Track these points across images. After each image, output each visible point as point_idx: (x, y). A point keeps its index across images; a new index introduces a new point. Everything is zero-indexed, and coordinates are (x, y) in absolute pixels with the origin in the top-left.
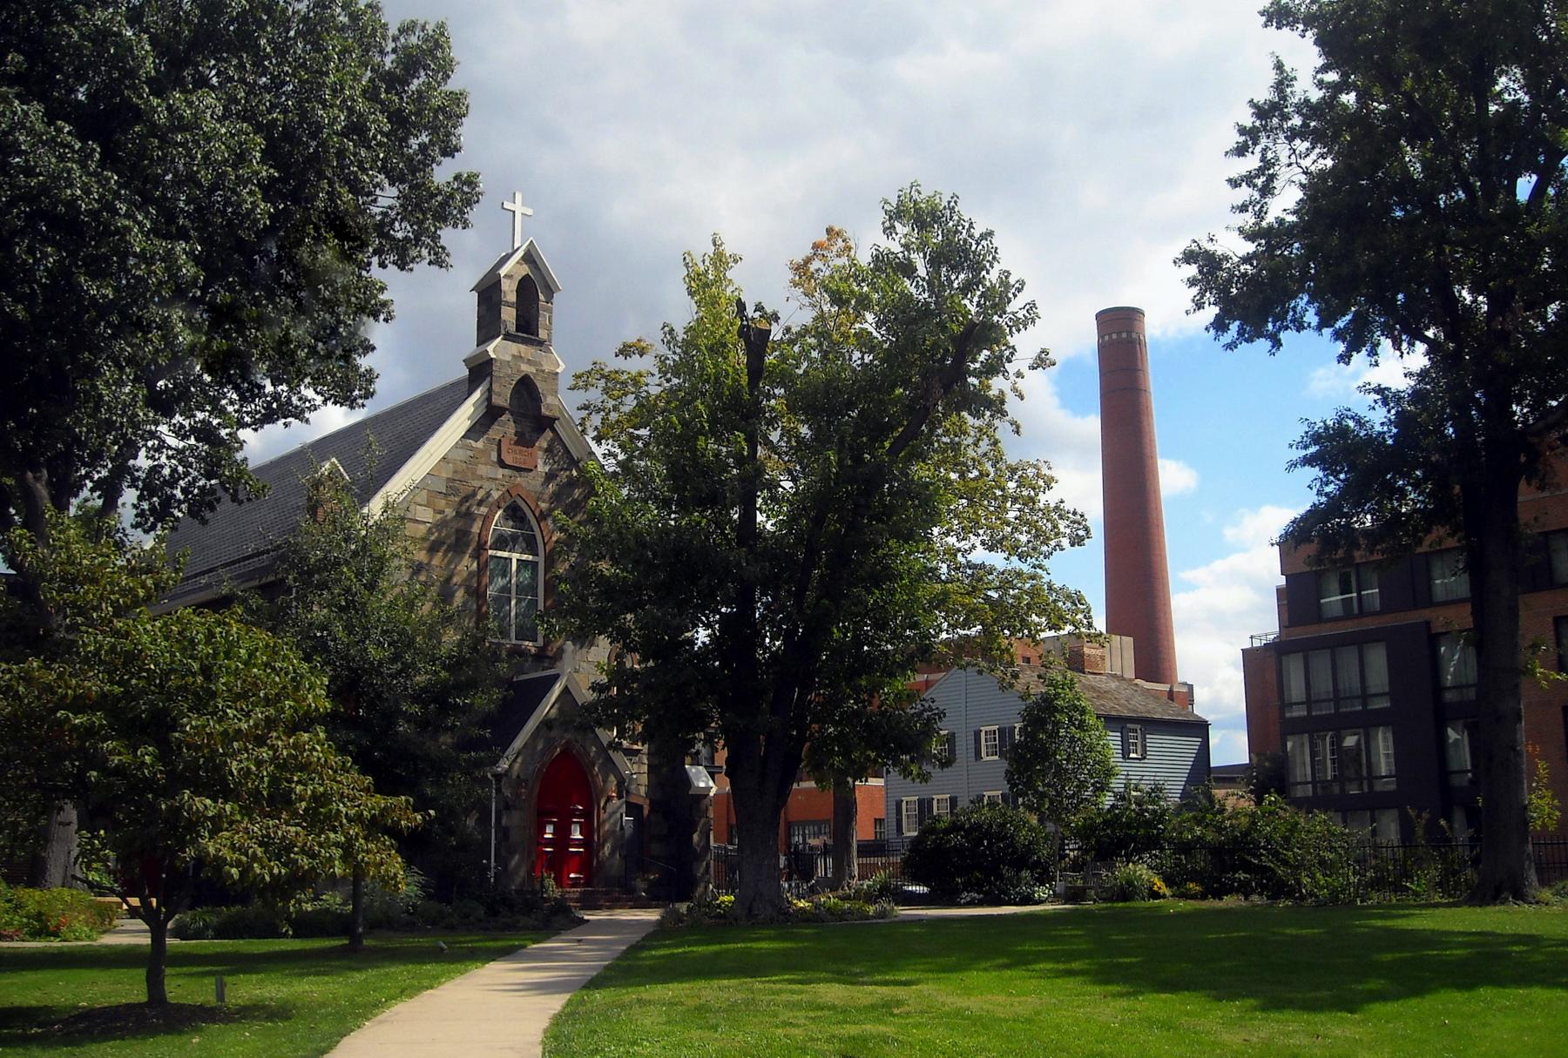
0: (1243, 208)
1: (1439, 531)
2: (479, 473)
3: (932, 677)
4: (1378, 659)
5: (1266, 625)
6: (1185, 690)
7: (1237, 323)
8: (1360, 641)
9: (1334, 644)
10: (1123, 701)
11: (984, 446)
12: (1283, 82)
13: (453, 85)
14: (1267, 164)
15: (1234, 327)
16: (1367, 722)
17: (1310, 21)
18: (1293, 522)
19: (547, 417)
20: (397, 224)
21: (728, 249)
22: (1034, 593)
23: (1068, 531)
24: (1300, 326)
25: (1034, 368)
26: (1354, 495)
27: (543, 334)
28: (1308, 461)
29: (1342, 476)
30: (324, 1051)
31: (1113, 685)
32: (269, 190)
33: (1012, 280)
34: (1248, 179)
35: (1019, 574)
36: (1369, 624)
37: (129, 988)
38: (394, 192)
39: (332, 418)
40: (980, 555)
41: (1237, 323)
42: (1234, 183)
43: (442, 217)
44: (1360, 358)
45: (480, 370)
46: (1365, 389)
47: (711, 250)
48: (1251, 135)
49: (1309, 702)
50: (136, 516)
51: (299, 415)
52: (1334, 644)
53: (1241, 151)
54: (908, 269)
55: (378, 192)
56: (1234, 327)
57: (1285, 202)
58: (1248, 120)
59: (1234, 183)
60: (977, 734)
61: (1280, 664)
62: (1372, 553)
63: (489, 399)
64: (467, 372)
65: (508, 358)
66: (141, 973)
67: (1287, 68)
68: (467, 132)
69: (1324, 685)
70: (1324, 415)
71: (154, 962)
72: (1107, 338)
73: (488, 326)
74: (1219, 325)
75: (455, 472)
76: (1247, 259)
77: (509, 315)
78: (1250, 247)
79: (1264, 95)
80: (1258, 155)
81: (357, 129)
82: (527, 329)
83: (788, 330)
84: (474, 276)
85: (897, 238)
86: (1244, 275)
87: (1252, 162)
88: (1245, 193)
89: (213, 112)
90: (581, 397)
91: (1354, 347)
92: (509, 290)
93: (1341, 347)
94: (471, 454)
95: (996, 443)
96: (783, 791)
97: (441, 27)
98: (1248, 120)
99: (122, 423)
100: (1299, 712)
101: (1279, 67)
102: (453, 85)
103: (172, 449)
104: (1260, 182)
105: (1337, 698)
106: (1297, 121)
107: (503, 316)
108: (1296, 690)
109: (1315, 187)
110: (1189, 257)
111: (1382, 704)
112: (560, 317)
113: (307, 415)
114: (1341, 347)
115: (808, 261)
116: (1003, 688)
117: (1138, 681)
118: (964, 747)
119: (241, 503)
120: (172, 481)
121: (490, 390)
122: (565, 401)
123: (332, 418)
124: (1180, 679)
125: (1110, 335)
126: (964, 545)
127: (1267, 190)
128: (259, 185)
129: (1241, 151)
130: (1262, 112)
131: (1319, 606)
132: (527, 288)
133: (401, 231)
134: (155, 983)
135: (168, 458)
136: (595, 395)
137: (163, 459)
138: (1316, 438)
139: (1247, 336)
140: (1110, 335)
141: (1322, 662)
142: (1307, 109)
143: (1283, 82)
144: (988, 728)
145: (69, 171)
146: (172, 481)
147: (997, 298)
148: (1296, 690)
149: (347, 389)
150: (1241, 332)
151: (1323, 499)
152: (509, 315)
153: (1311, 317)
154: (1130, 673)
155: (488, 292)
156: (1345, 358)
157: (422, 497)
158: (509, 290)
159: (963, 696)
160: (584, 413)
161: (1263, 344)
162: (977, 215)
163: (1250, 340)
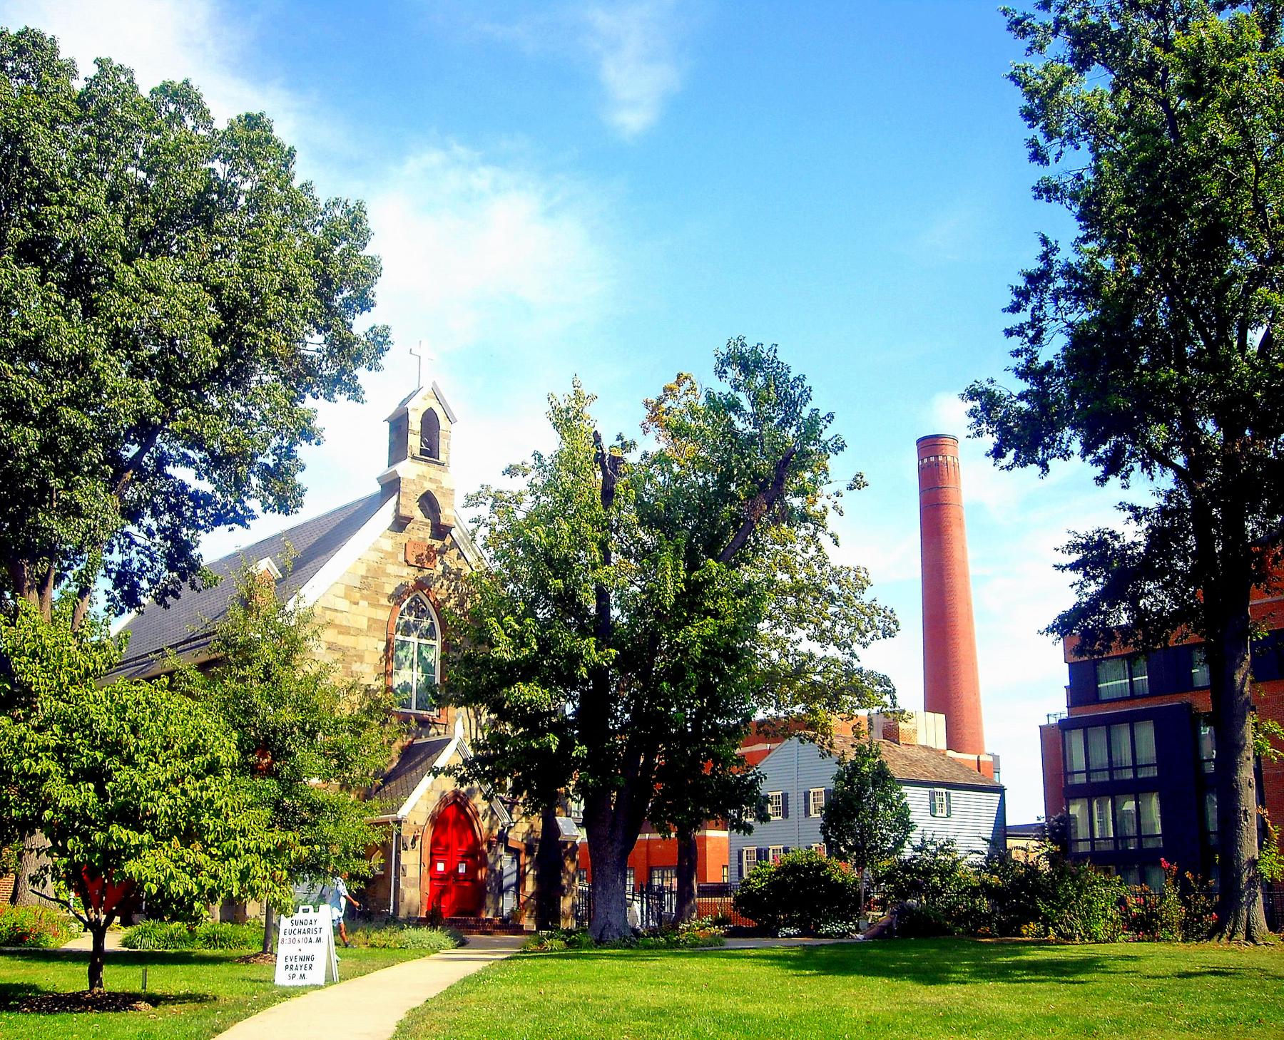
0: (1017, 353)
1: (1183, 628)
2: (388, 571)
3: (774, 746)
4: (1146, 734)
5: (1058, 706)
6: (990, 759)
7: (1014, 451)
8: (1132, 719)
9: (1109, 722)
10: (931, 769)
11: (812, 551)
12: (1049, 249)
13: (368, 251)
14: (1035, 322)
15: (1010, 455)
16: (1137, 788)
17: (1074, 197)
18: (1059, 617)
19: (445, 526)
20: (324, 363)
21: (586, 391)
22: (849, 674)
23: (881, 625)
24: (1066, 455)
25: (851, 489)
26: (1112, 594)
27: (442, 458)
28: (1074, 567)
29: (1101, 580)
30: (218, 1031)
31: (924, 754)
32: (217, 336)
33: (822, 414)
34: (1020, 331)
35: (835, 661)
36: (1141, 706)
37: (72, 979)
38: (319, 339)
39: (268, 524)
40: (806, 646)
41: (1014, 451)
42: (1009, 333)
43: (357, 358)
44: (1114, 481)
45: (391, 486)
46: (1122, 506)
47: (571, 391)
48: (1023, 294)
49: (1088, 771)
50: (108, 601)
51: (241, 521)
52: (1109, 722)
53: (1015, 308)
54: (734, 406)
55: (307, 338)
56: (1010, 455)
57: (1053, 348)
58: (1021, 283)
59: (1009, 333)
60: (807, 795)
61: (1063, 736)
62: (1125, 644)
63: (397, 510)
64: (379, 488)
65: (414, 477)
66: (84, 968)
67: (1051, 240)
68: (381, 291)
69: (1100, 758)
70: (1087, 527)
71: (97, 959)
72: (926, 460)
73: (398, 450)
74: (998, 453)
75: (368, 570)
76: (1022, 397)
77: (415, 442)
78: (1024, 386)
79: (1035, 265)
80: (1029, 312)
81: (290, 290)
82: (430, 452)
83: (645, 455)
84: (390, 409)
85: (728, 381)
86: (1019, 410)
87: (1024, 317)
88: (1016, 342)
89: (173, 274)
90: (473, 512)
91: (1108, 472)
92: (415, 423)
93: (1099, 470)
94: (382, 555)
95: (819, 550)
96: (630, 841)
97: (360, 205)
98: (1021, 283)
99: (95, 526)
100: (1080, 779)
101: (1045, 241)
102: (368, 251)
103: (139, 545)
104: (1031, 333)
105: (1111, 768)
106: (1061, 283)
107: (410, 443)
108: (1078, 762)
109: (1079, 337)
110: (973, 394)
111: (1153, 772)
112: (452, 441)
113: (247, 522)
114: (1099, 470)
115: (661, 401)
116: (822, 756)
117: (951, 753)
118: (796, 809)
119: (199, 591)
120: (141, 573)
121: (398, 503)
122: (456, 513)
123: (268, 524)
124: (988, 749)
125: (928, 458)
126: (793, 637)
127: (1036, 340)
128: (210, 333)
129: (1015, 308)
130: (1031, 278)
131: (1097, 690)
132: (430, 421)
133: (328, 370)
134: (94, 976)
135: (138, 553)
136: (484, 511)
137: (133, 554)
138: (1074, 547)
139: (1021, 462)
140: (928, 458)
141: (1098, 737)
142: (1070, 272)
143: (1049, 249)
144: (816, 790)
145: (57, 322)
146: (141, 573)
147: (811, 429)
148: (1078, 762)
149: (285, 501)
150: (1017, 458)
151: (1085, 599)
152: (415, 442)
153: (1076, 446)
154: (942, 744)
155: (398, 425)
156: (1101, 481)
157: (340, 590)
158: (415, 423)
159: (796, 759)
160: (474, 526)
161: (1034, 469)
162: (795, 360)
163: (1024, 465)
